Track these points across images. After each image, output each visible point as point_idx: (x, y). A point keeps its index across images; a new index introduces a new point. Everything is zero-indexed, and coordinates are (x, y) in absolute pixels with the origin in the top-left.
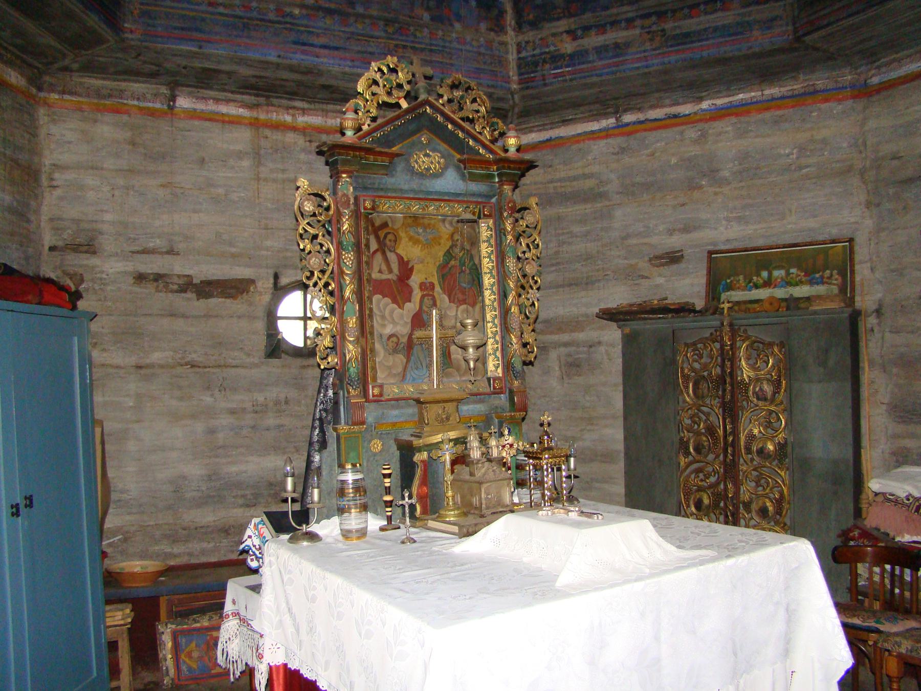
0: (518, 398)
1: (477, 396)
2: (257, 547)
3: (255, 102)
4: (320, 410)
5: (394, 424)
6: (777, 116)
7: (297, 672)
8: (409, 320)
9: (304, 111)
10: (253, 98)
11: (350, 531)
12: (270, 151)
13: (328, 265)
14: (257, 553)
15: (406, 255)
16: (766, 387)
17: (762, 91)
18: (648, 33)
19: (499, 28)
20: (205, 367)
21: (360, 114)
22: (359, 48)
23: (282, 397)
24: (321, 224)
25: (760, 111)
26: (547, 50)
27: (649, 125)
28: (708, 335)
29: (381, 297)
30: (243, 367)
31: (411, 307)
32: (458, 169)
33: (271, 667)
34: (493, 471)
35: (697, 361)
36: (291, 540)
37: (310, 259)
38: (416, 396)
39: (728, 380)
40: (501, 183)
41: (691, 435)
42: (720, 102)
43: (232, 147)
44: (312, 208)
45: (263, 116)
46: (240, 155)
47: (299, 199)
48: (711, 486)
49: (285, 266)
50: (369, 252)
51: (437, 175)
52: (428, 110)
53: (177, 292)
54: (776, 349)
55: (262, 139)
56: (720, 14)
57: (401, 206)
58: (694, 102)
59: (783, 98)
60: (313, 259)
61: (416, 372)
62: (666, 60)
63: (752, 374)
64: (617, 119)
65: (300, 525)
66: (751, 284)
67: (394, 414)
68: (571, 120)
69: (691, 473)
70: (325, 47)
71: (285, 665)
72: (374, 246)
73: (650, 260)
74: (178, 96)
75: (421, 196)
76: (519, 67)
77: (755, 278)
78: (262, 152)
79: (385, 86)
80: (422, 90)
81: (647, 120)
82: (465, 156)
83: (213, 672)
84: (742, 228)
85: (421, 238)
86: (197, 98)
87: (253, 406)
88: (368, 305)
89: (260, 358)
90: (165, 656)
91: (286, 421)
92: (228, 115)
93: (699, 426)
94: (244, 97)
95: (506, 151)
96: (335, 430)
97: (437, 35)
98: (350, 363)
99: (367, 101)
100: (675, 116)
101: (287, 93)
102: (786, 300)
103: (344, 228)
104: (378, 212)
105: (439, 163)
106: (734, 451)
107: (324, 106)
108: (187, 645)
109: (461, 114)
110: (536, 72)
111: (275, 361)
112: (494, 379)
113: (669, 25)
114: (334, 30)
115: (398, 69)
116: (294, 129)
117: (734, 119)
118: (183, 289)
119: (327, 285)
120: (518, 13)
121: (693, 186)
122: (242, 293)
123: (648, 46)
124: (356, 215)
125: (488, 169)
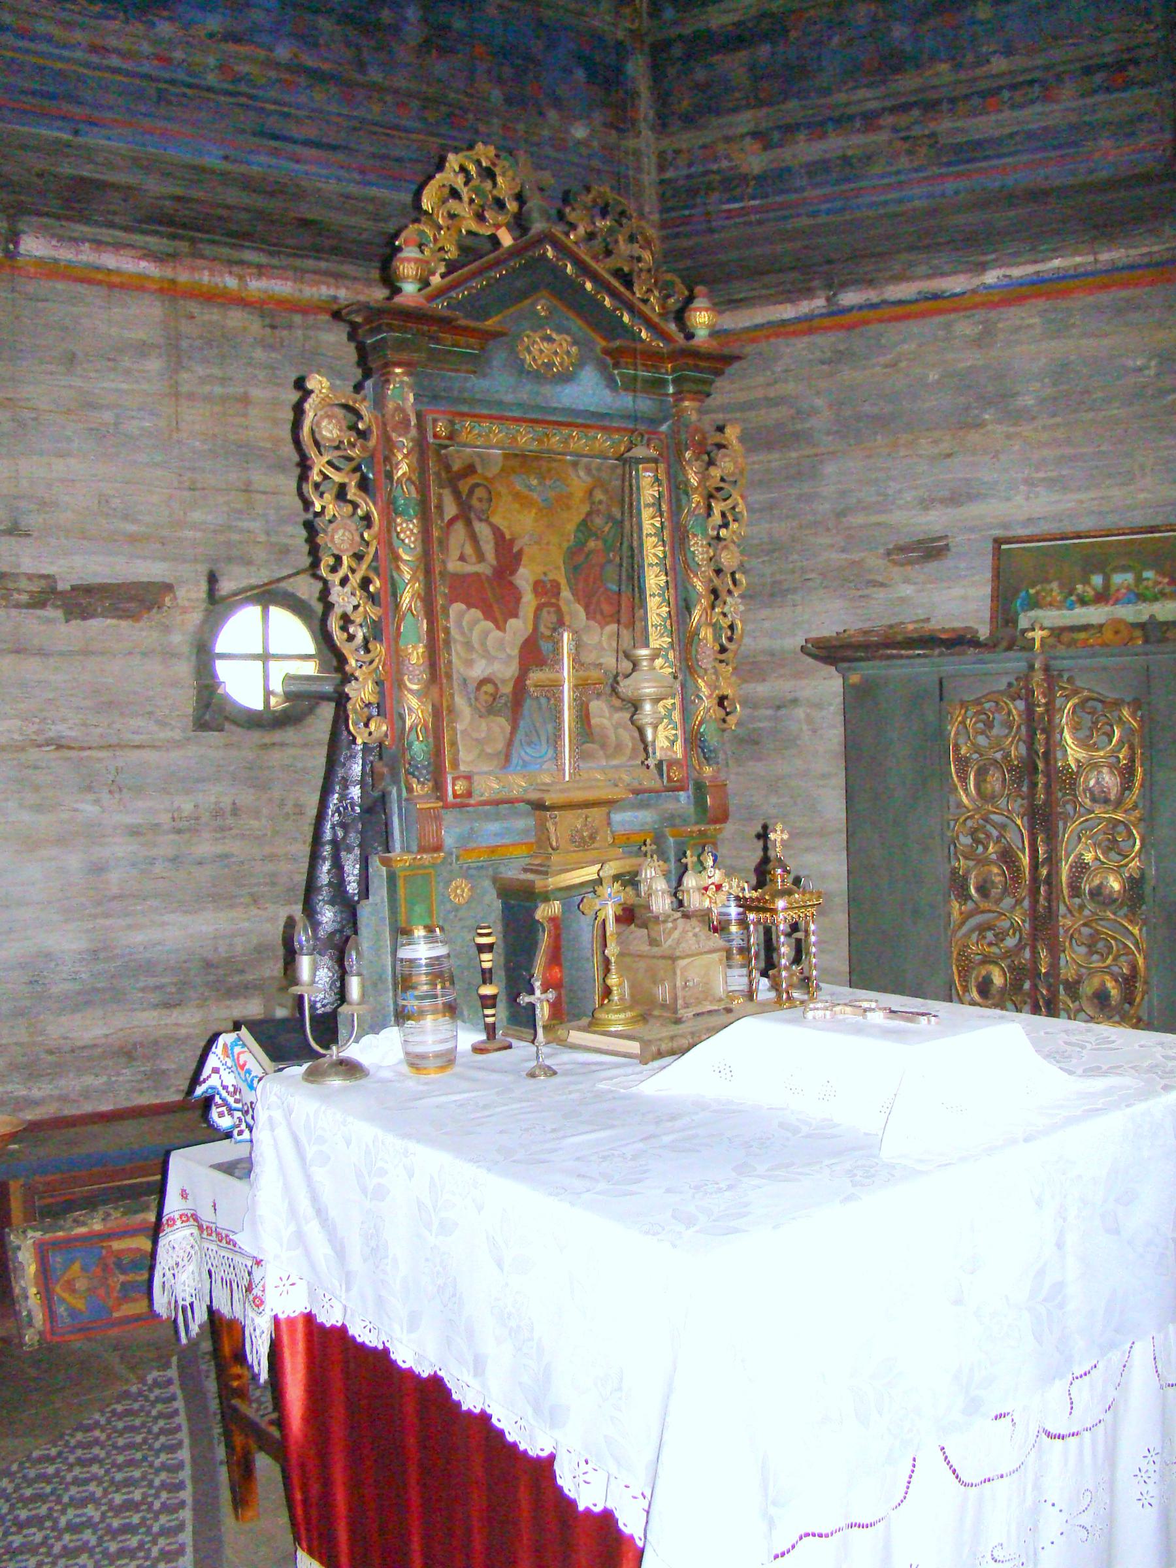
0: (713, 798)
1: (641, 797)
2: (231, 1089)
3: (171, 250)
4: (333, 827)
5: (493, 850)
6: (1121, 299)
7: (340, 1333)
8: (515, 652)
9: (261, 270)
10: (165, 241)
11: (423, 1057)
12: (198, 343)
13: (368, 544)
14: (231, 1100)
15: (509, 527)
16: (1107, 778)
17: (1095, 254)
18: (904, 139)
19: (622, 122)
20: (82, 749)
21: (427, 252)
22: (375, 150)
23: (226, 802)
24: (354, 464)
25: (1091, 290)
26: (715, 167)
27: (886, 312)
28: (1002, 686)
29: (463, 607)
30: (154, 747)
31: (519, 627)
32: (602, 368)
33: (276, 1319)
34: (695, 935)
35: (983, 733)
36: (313, 1076)
37: (335, 531)
38: (534, 796)
39: (1041, 766)
40: (679, 396)
41: (971, 863)
42: (1016, 272)
43: (126, 334)
44: (336, 432)
45: (184, 277)
46: (142, 349)
47: (311, 414)
48: (1007, 955)
49: (229, 559)
50: (442, 519)
51: (566, 377)
52: (550, 254)
53: (29, 606)
54: (1126, 712)
55: (184, 321)
56: (1038, 108)
57: (498, 433)
58: (970, 271)
59: (1131, 267)
60: (341, 532)
61: (529, 750)
62: (937, 189)
63: (1082, 754)
64: (828, 299)
65: (327, 1048)
66: (1073, 598)
67: (491, 830)
68: (741, 300)
69: (972, 931)
70: (308, 143)
71: (309, 1318)
72: (451, 510)
73: (889, 553)
74: (24, 232)
75: (534, 416)
76: (662, 198)
77: (1079, 587)
78: (184, 344)
79: (472, 201)
80: (535, 215)
81: (885, 302)
82: (618, 343)
83: (116, 1315)
84: (1056, 497)
85: (535, 495)
86: (61, 239)
87: (173, 819)
88: (442, 622)
89: (184, 730)
90: (24, 1289)
91: (235, 847)
92: (118, 272)
93: (986, 848)
94: (148, 239)
95: (690, 336)
96: (386, 862)
97: (515, 131)
98: (413, 732)
99: (440, 228)
100: (936, 297)
101: (230, 234)
102: (1142, 626)
103: (400, 473)
104: (459, 444)
105: (568, 353)
106: (1049, 895)
107: (298, 262)
108: (67, 1268)
109: (613, 262)
110: (694, 207)
111: (212, 736)
112: (671, 764)
113: (944, 125)
114: (329, 113)
115: (497, 170)
116: (240, 302)
117: (1041, 304)
118: (39, 601)
119: (365, 583)
120: (662, 98)
121: (966, 423)
122: (149, 609)
123: (903, 162)
124: (421, 447)
125: (657, 369)
